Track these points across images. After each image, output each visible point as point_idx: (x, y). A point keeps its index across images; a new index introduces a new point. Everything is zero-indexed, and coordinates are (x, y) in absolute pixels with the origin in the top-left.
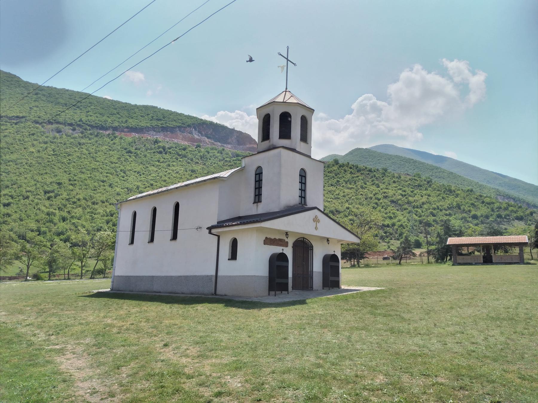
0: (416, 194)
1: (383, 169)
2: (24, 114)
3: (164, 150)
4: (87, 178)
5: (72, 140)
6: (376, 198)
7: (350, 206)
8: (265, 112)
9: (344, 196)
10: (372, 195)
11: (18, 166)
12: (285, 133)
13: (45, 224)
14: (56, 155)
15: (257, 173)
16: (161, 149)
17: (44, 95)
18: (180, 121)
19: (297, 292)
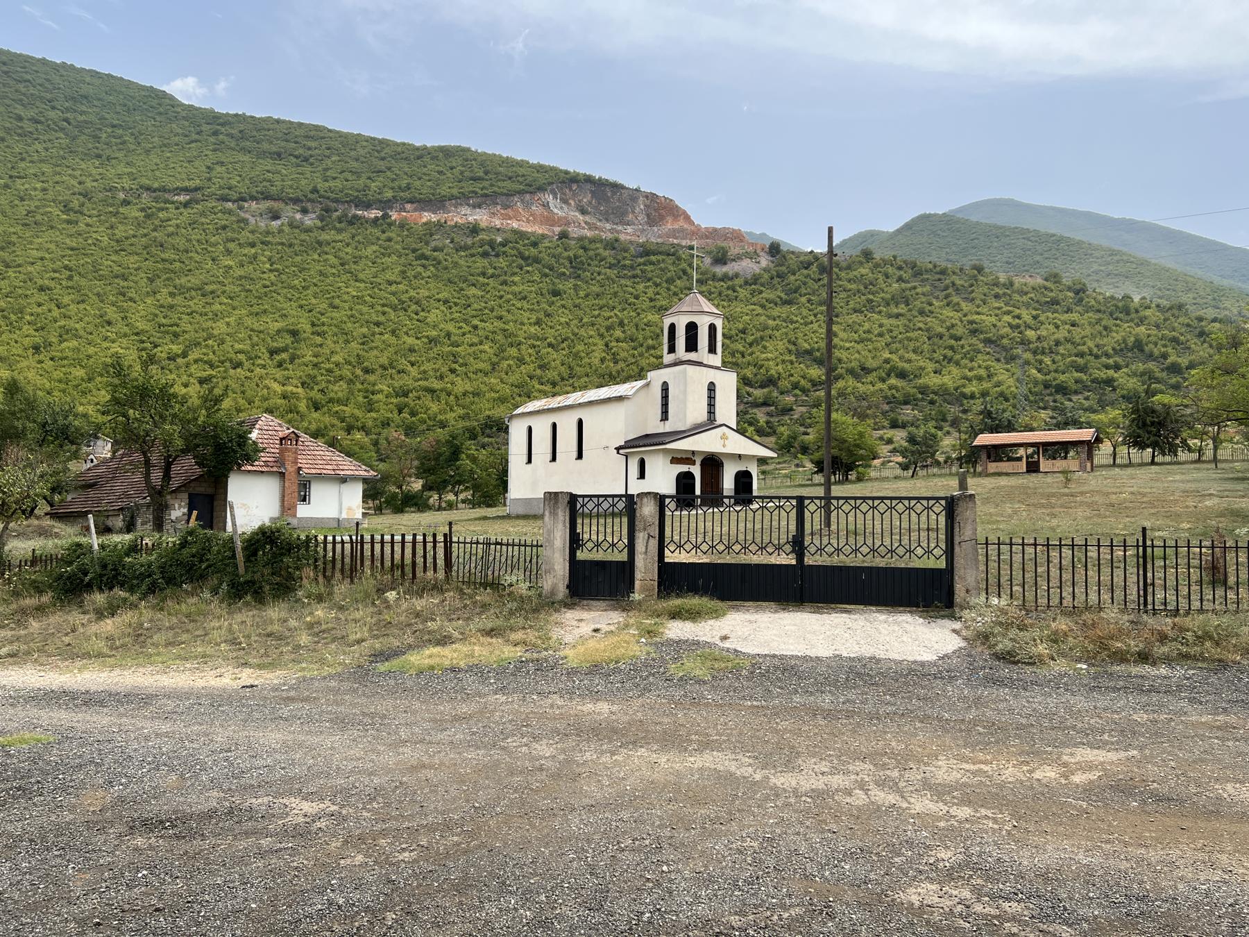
0: (1042, 324)
3: (493, 249)
5: (304, 236)
7: (893, 357)
9: (881, 335)
12: (692, 345)
14: (277, 270)
18: (521, 179)
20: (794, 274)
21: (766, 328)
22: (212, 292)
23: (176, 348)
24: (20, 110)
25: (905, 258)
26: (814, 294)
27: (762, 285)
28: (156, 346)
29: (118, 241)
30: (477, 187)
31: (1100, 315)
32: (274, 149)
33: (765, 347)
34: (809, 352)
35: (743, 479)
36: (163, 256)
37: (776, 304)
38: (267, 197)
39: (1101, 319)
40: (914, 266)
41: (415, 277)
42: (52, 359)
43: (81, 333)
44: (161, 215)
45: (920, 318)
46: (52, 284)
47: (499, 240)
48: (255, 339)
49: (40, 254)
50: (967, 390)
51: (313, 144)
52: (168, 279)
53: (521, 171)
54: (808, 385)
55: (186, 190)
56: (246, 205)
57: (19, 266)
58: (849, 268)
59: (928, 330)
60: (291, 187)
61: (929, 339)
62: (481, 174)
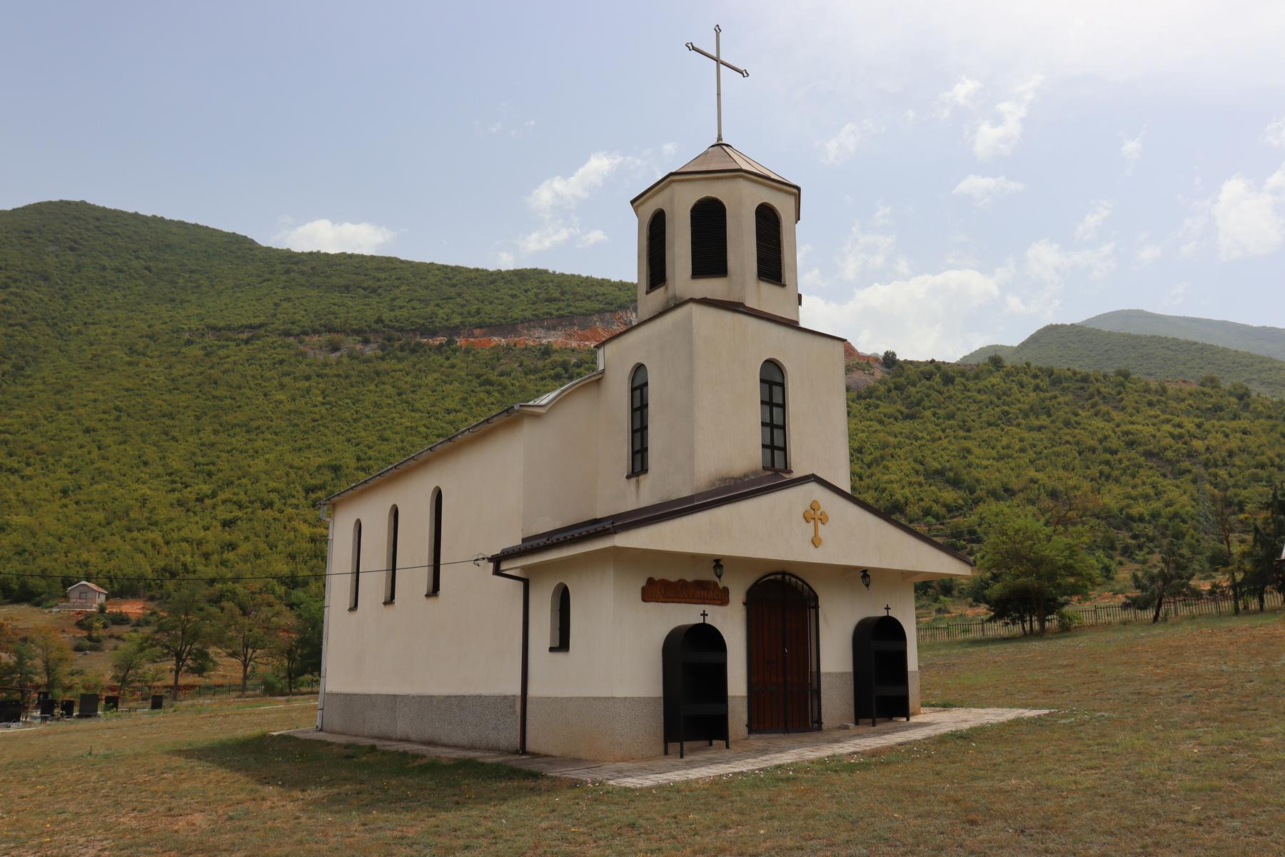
0: (1208, 432)
1: (1119, 373)
2: (263, 319)
3: (566, 370)
4: (394, 452)
5: (363, 367)
6: (1107, 450)
7: (1039, 476)
8: (650, 208)
9: (1023, 450)
10: (1094, 443)
11: (253, 436)
12: (710, 260)
13: (306, 563)
14: (329, 403)
15: (636, 384)
16: (559, 369)
17: (303, 273)
18: (600, 298)
19: (758, 741)
20: (914, 385)
21: (885, 446)
22: (258, 428)
23: (206, 489)
24: (105, 261)
25: (1040, 365)
26: (939, 407)
27: (879, 398)
28: (186, 487)
29: (173, 380)
30: (552, 308)
31: (1274, 422)
32: (343, 282)
33: (887, 468)
34: (939, 473)
35: (879, 646)
36: (215, 393)
37: (896, 419)
38: (330, 330)
39: (1275, 426)
40: (1050, 373)
41: (477, 404)
42: (77, 503)
43: (115, 474)
44: (220, 352)
45: (1066, 430)
46: (99, 426)
47: (574, 360)
48: (293, 476)
49: (91, 396)
50: (1134, 511)
51: (382, 275)
52: (215, 416)
53: (600, 290)
54: (943, 511)
55: (250, 327)
56: (307, 339)
57: (71, 408)
58: (977, 377)
59: (1077, 443)
60: (355, 318)
61: (1080, 453)
62: (557, 295)
